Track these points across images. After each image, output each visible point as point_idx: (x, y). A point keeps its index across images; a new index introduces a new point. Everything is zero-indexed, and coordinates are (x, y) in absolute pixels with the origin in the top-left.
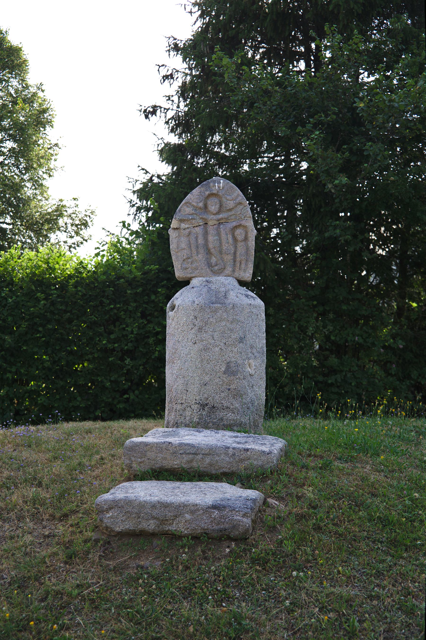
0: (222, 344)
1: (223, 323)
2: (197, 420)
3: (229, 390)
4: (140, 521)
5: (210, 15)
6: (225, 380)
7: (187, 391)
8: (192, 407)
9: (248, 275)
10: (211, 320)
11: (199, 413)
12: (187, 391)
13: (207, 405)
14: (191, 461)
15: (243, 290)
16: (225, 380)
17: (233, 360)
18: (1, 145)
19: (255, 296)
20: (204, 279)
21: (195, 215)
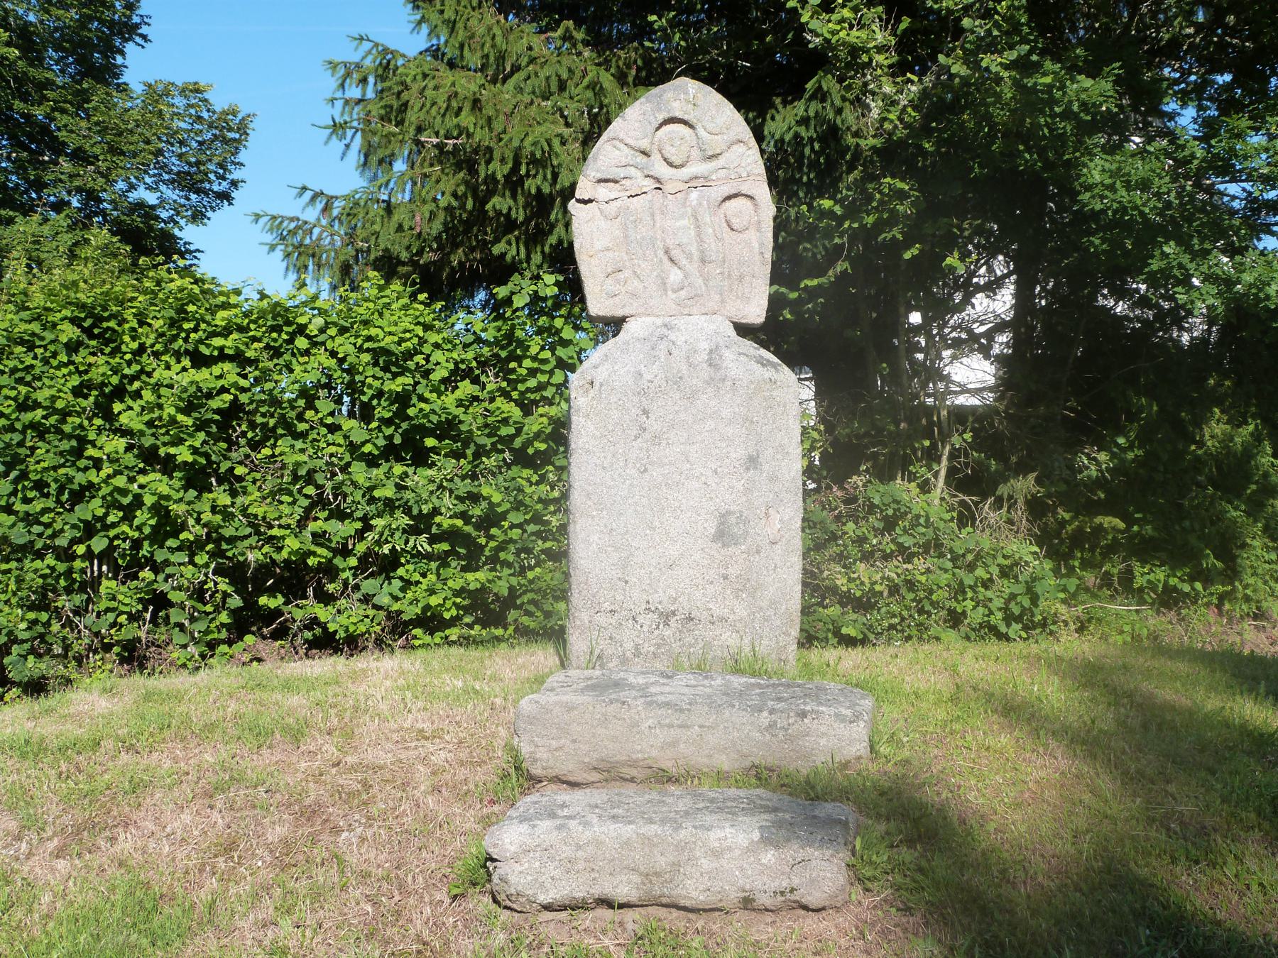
0: (709, 473)
1: (711, 424)
2: (652, 649)
3: (725, 578)
4: (594, 879)
5: (1129, 526)
6: (717, 555)
7: (626, 582)
8: (640, 619)
9: (756, 313)
10: (682, 416)
11: (656, 632)
12: (626, 582)
13: (674, 613)
14: (674, 744)
15: (748, 346)
16: (717, 555)
17: (733, 508)
18: (1255, 712)
19: (776, 360)
20: (659, 321)
21: (632, 169)
